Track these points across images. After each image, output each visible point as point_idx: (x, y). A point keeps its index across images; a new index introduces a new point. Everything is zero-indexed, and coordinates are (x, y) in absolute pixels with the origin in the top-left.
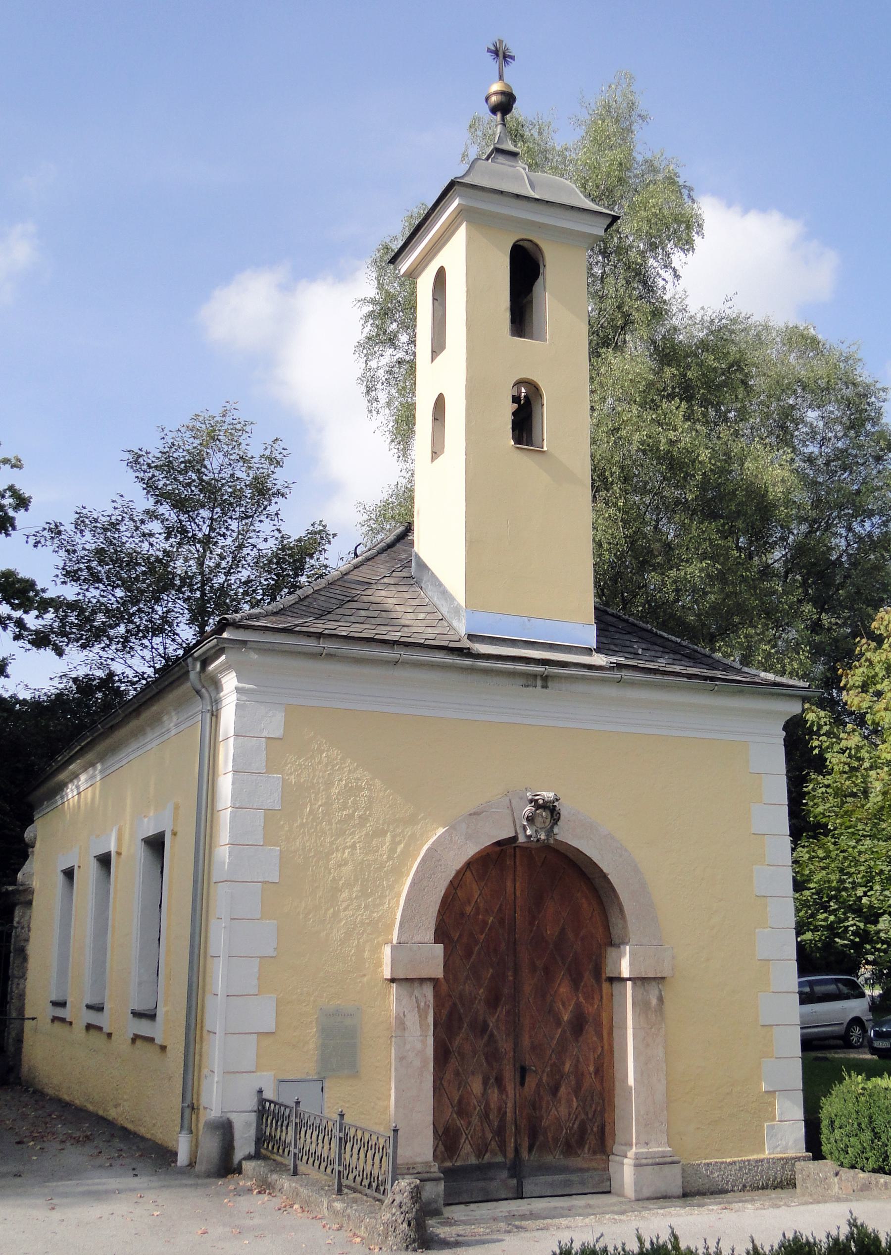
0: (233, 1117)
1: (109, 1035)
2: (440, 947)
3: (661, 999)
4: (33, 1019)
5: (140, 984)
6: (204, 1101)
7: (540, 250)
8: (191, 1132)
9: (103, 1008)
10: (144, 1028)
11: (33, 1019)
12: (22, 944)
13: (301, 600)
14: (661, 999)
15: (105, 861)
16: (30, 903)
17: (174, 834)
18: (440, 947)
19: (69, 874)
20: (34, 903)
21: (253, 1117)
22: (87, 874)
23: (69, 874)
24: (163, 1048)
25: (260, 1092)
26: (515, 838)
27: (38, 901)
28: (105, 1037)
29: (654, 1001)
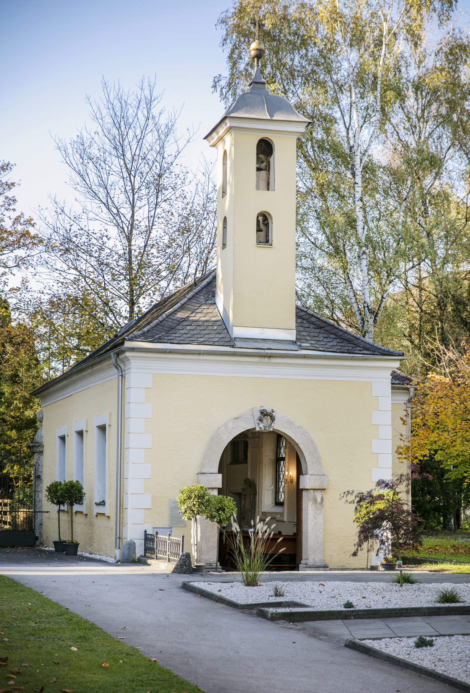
0: (135, 541)
1: (86, 515)
2: (220, 475)
3: (322, 499)
4: (47, 512)
5: (98, 491)
6: (124, 536)
7: (272, 142)
8: (120, 548)
9: (268, 189)
10: (100, 509)
11: (47, 512)
12: (39, 473)
13: (161, 322)
14: (322, 499)
15: (80, 434)
16: (42, 452)
17: (110, 426)
18: (220, 475)
19: (63, 438)
20: (44, 452)
21: (143, 541)
22: (72, 440)
23: (63, 438)
24: (109, 517)
25: (146, 531)
26: (255, 428)
27: (46, 450)
28: (84, 516)
29: (319, 500)
